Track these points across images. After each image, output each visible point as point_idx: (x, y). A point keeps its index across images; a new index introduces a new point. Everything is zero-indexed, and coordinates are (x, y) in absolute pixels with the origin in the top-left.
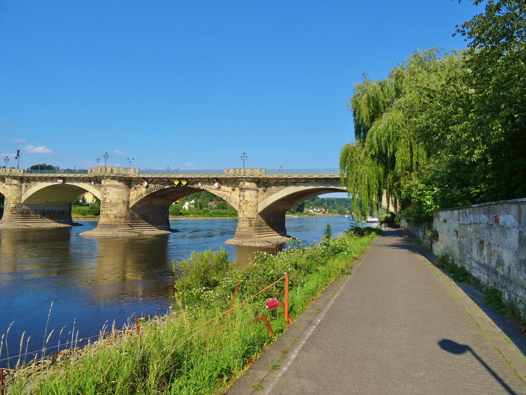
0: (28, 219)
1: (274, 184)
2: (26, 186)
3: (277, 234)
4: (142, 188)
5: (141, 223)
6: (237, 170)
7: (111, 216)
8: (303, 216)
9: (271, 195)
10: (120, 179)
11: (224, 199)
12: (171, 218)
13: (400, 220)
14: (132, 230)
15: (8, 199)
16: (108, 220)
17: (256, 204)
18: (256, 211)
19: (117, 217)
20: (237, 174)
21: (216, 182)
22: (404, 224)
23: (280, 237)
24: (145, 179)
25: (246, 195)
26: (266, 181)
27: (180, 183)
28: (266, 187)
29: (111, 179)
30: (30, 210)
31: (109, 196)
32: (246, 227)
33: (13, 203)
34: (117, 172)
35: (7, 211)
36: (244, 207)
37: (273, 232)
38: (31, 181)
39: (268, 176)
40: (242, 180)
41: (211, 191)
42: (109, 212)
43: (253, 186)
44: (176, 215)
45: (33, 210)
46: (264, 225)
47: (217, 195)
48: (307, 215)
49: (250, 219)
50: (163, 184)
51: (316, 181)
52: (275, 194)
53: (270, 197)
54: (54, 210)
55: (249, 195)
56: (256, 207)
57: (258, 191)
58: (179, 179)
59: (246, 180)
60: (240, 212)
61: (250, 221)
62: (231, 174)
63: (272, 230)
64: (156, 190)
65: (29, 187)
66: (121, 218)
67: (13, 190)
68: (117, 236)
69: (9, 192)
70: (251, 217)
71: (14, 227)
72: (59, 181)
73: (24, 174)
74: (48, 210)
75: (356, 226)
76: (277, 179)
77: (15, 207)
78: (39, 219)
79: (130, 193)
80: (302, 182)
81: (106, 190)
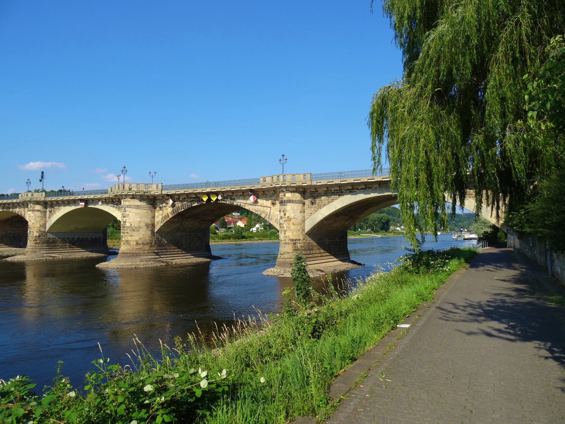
0: (55, 249)
1: (325, 193)
2: (50, 212)
3: (336, 259)
4: (167, 207)
5: (172, 250)
6: (275, 178)
7: (132, 243)
8: (388, 234)
9: (320, 209)
10: (142, 198)
11: (263, 216)
12: (212, 243)
13: (506, 235)
14: (158, 259)
15: (31, 227)
16: (129, 247)
17: (301, 221)
18: (302, 230)
19: (140, 244)
20: (274, 183)
21: (251, 195)
22: (513, 241)
23: (340, 262)
24: (171, 196)
25: (288, 209)
26: (314, 190)
27: (209, 200)
28: (314, 198)
29: (131, 198)
30: (57, 238)
32: (289, 251)
33: (37, 232)
34: (136, 189)
35: (30, 241)
36: (285, 225)
37: (328, 257)
38: (54, 205)
39: (314, 183)
40: (282, 191)
41: (247, 207)
42: (129, 238)
43: (296, 197)
44: (238, 239)
45: (60, 238)
46: (315, 248)
47: (254, 211)
48: (393, 234)
49: (294, 242)
50: (191, 202)
51: (380, 187)
52: (326, 206)
54: (85, 238)
55: (292, 210)
56: (302, 225)
57: (304, 204)
58: (208, 194)
59: (287, 189)
60: (281, 233)
61: (295, 244)
62: (268, 183)
63: (327, 254)
64: (184, 209)
65: (53, 212)
66: (145, 244)
67: (37, 216)
68: (137, 266)
69: (32, 219)
70: (296, 238)
71: (37, 259)
72: (81, 204)
73: (46, 198)
74: (78, 238)
75: (419, 250)
76: (327, 186)
77: (39, 236)
78: (68, 249)
79: (155, 215)
80: (361, 189)
81: (125, 211)
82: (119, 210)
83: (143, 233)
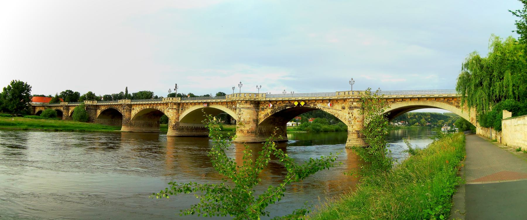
4: (268, 109)
6: (347, 93)
19: (250, 132)
27: (299, 104)
33: (174, 122)
42: (243, 129)
54: (198, 127)
61: (358, 133)
73: (181, 101)
81: (241, 111)
82: (231, 110)
83: (252, 125)
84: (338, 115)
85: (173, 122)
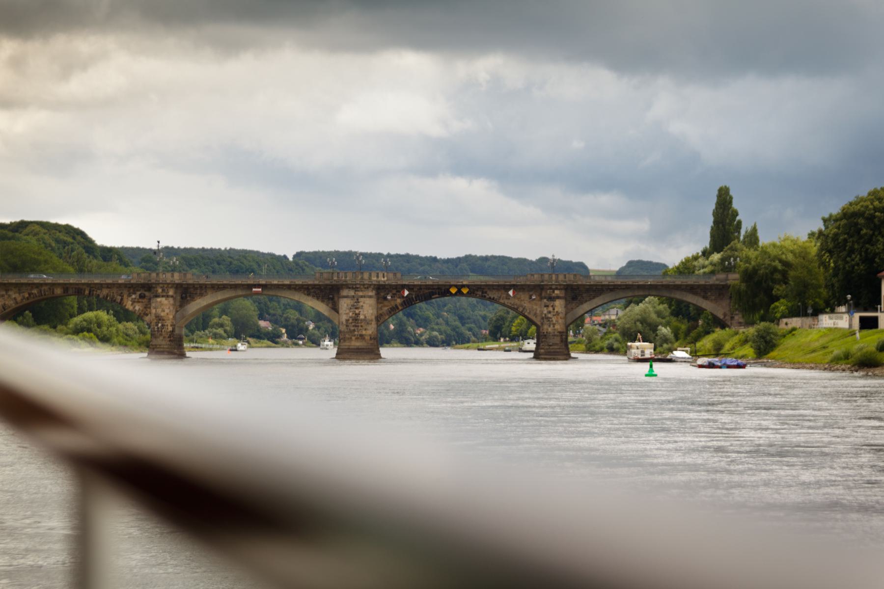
4: (396, 298)
7: (366, 338)
25: (556, 305)
31: (363, 311)
42: (364, 332)
52: (588, 303)
53: (581, 306)
81: (359, 302)
84: (524, 309)
85: (169, 325)
